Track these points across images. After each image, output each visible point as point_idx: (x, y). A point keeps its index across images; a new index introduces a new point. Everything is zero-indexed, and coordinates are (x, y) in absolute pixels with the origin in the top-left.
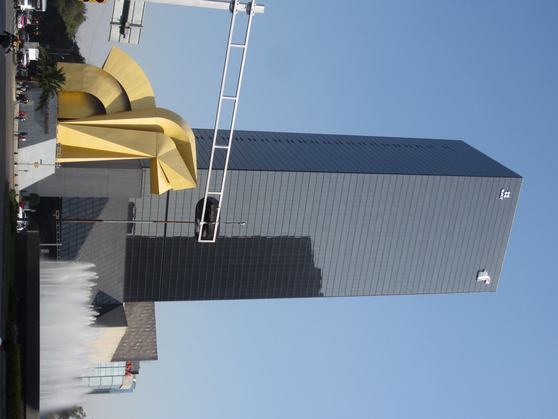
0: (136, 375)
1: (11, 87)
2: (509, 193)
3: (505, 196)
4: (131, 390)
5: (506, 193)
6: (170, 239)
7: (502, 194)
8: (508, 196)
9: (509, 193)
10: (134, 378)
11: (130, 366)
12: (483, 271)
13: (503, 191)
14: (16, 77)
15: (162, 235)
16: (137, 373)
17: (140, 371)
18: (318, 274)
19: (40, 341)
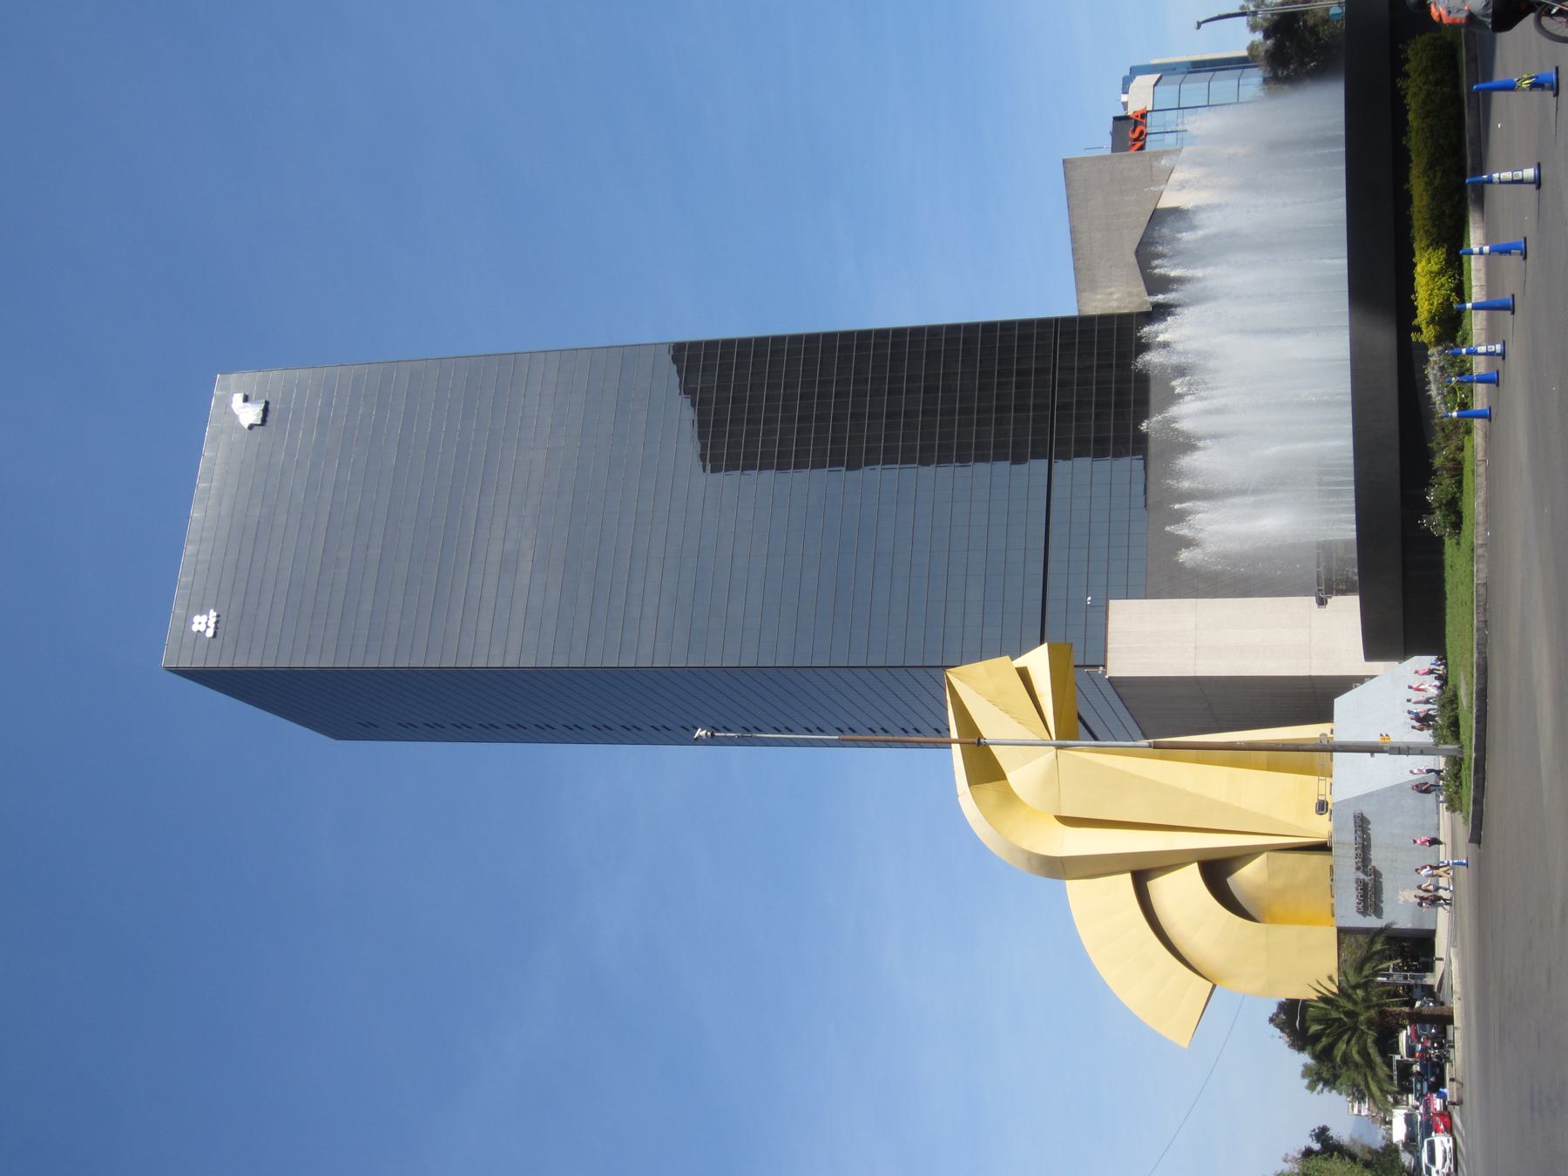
0: (1122, 113)
1: (1465, 998)
2: (195, 628)
3: (204, 618)
4: (1136, 71)
5: (202, 628)
6: (1036, 455)
7: (211, 624)
8: (197, 619)
9: (195, 628)
10: (1125, 105)
11: (1136, 134)
12: (251, 427)
13: (210, 633)
14: (1451, 1022)
15: (1060, 466)
16: (1116, 119)
17: (1109, 125)
18: (675, 359)
19: (1343, 111)
